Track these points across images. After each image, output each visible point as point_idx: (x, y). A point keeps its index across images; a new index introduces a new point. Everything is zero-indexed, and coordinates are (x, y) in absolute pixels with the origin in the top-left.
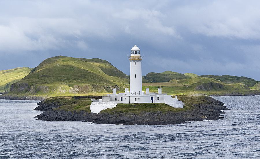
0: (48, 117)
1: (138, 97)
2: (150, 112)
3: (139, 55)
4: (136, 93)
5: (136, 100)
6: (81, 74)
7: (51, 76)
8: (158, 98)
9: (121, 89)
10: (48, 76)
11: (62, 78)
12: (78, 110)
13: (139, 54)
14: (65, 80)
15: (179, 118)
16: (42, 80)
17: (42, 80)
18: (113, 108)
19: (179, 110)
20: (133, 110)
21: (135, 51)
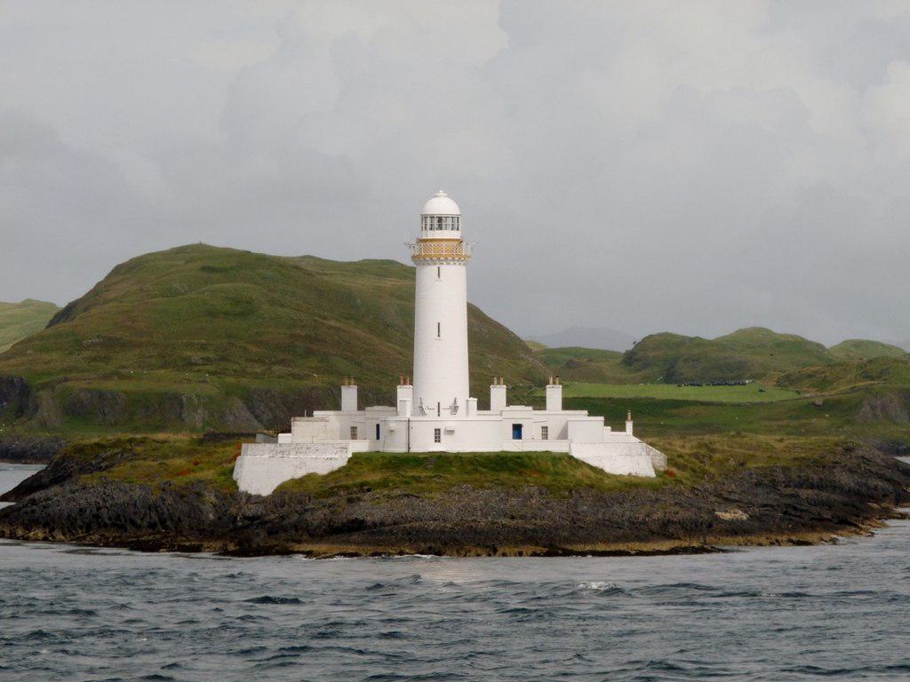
0: (45, 507)
1: (447, 421)
2: (490, 488)
3: (456, 235)
4: (444, 411)
5: (437, 439)
6: (292, 336)
7: (140, 345)
8: (545, 429)
9: (379, 394)
10: (125, 345)
11: (196, 356)
12: (179, 481)
13: (455, 232)
14: (207, 361)
15: (616, 518)
16: (94, 359)
17: (94, 359)
18: (333, 473)
19: (630, 487)
20: (417, 479)
21: (440, 219)
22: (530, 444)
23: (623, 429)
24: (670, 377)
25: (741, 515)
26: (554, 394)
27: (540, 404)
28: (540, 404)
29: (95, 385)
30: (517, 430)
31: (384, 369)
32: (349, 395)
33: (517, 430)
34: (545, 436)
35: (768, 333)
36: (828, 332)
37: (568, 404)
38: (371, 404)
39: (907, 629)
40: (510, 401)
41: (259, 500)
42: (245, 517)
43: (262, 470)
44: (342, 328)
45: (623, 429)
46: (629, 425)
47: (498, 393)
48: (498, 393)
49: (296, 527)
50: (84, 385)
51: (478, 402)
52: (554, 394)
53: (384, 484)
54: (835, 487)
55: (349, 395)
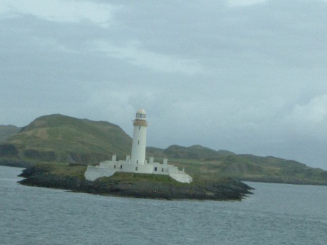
4: (140, 163)
8: (163, 169)
19: (184, 185)
22: (159, 172)
25: (212, 194)
26: (165, 161)
27: (162, 163)
29: (32, 148)
30: (156, 169)
32: (114, 157)
35: (15, 127)
37: (169, 163)
41: (90, 182)
42: (88, 186)
43: (91, 175)
44: (114, 140)
45: (182, 170)
46: (184, 170)
47: (152, 159)
48: (152, 159)
51: (168, 161)
52: (165, 161)
54: (231, 189)
55: (114, 157)
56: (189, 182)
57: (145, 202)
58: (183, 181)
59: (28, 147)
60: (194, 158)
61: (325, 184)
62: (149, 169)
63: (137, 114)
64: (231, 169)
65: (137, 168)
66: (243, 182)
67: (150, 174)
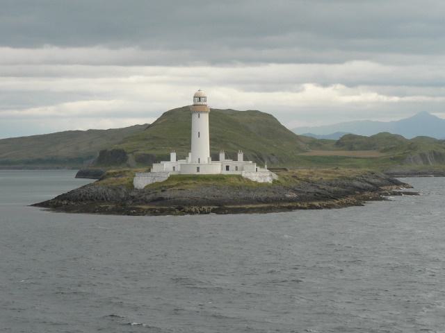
23: (264, 167)
24: (351, 149)
26: (240, 156)
27: (235, 159)
28: (235, 159)
29: (147, 152)
30: (227, 168)
31: (184, 146)
32: (173, 156)
33: (227, 168)
34: (237, 169)
36: (392, 133)
38: (179, 159)
39: (442, 245)
40: (226, 158)
46: (266, 166)
47: (222, 156)
48: (222, 156)
49: (142, 200)
50: (142, 152)
52: (240, 156)
53: (178, 185)
56: (271, 182)
57: (416, 198)
58: (261, 181)
59: (141, 152)
60: (375, 149)
61: (439, 174)
62: (217, 169)
63: (194, 97)
64: (412, 160)
65: (198, 168)
66: (397, 179)
67: (217, 175)
